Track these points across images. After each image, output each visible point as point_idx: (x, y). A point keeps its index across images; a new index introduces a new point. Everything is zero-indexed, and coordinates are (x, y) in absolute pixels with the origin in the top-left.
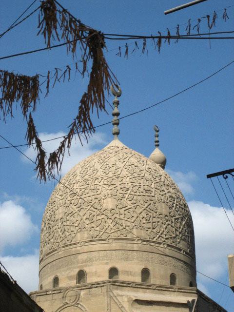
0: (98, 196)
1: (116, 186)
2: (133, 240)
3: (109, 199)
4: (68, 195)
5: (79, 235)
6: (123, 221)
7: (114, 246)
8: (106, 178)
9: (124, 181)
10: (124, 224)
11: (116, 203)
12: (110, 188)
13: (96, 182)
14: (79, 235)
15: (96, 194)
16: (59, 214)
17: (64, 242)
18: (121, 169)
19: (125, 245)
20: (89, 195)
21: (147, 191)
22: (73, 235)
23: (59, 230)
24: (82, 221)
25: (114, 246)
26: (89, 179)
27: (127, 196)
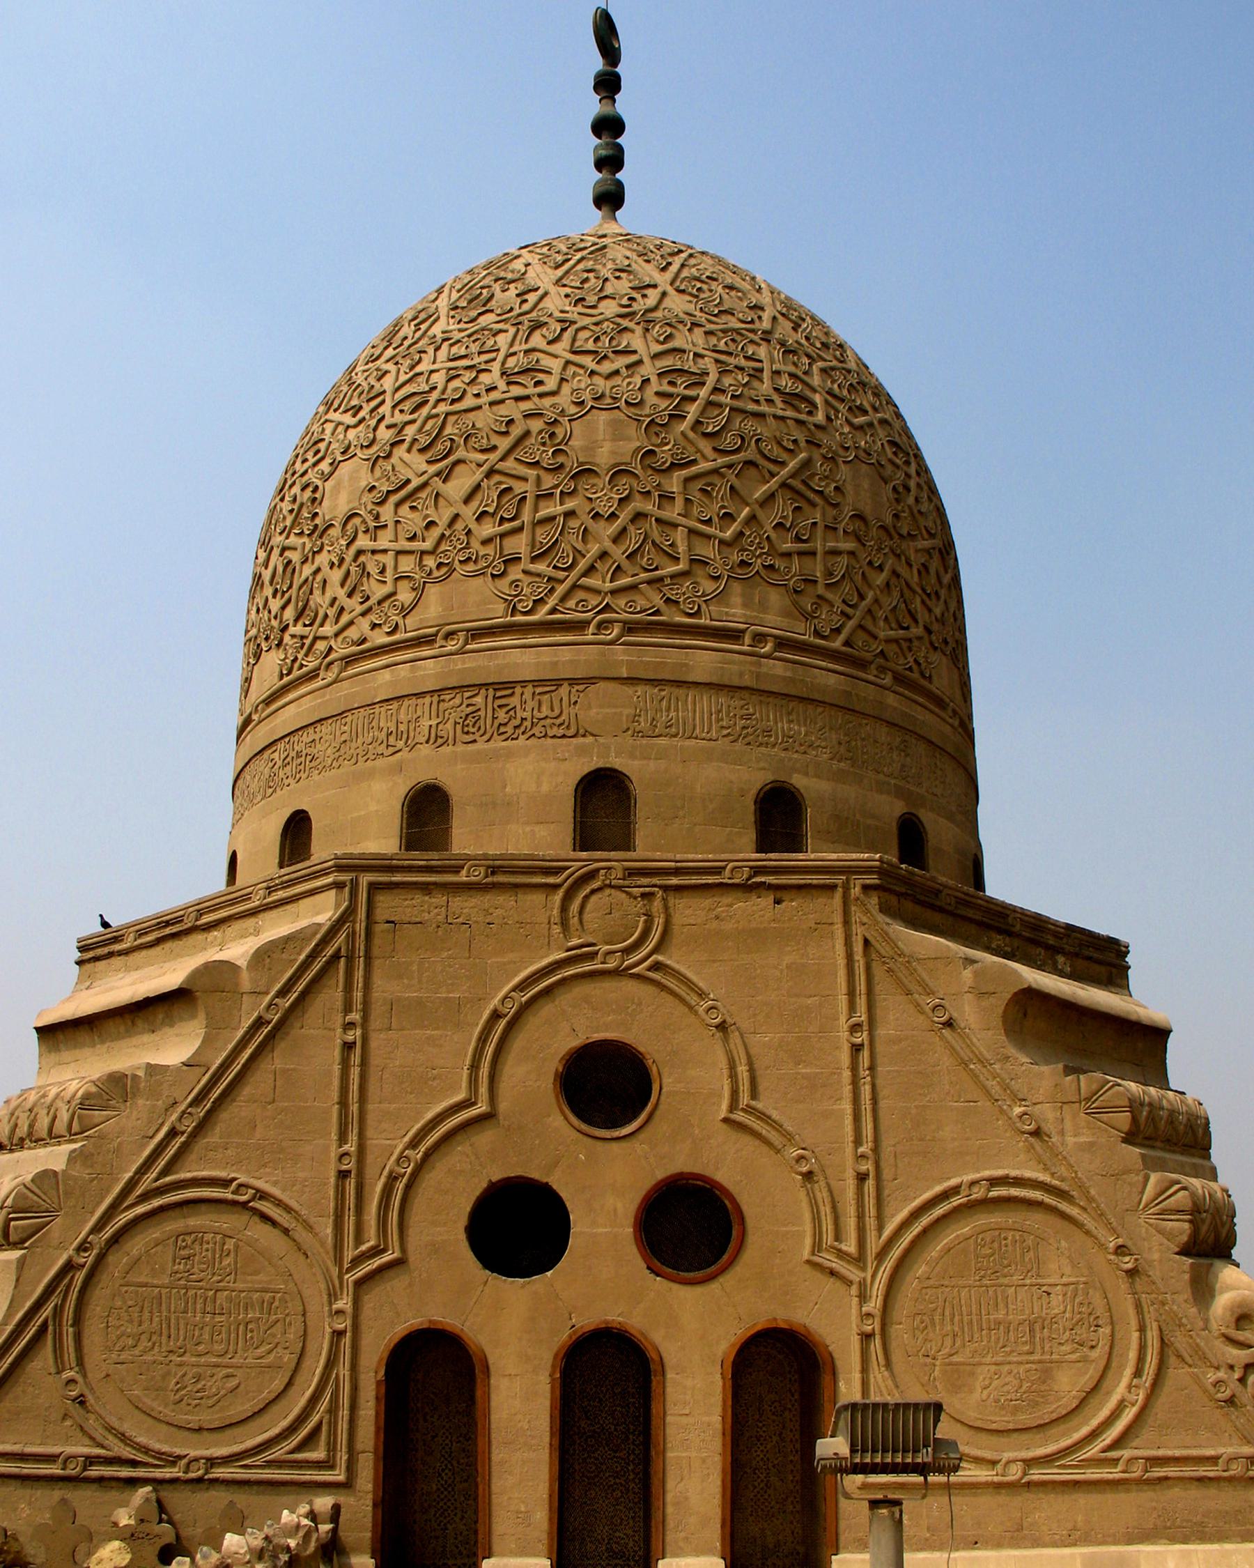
0: (547, 402)
1: (633, 358)
4: (389, 404)
6: (680, 536)
7: (623, 658)
8: (587, 321)
9: (676, 343)
10: (682, 548)
11: (635, 440)
12: (607, 367)
13: (537, 340)
15: (531, 390)
17: (353, 633)
18: (660, 290)
20: (495, 395)
21: (792, 399)
22: (405, 596)
24: (459, 526)
25: (623, 658)
27: (693, 410)
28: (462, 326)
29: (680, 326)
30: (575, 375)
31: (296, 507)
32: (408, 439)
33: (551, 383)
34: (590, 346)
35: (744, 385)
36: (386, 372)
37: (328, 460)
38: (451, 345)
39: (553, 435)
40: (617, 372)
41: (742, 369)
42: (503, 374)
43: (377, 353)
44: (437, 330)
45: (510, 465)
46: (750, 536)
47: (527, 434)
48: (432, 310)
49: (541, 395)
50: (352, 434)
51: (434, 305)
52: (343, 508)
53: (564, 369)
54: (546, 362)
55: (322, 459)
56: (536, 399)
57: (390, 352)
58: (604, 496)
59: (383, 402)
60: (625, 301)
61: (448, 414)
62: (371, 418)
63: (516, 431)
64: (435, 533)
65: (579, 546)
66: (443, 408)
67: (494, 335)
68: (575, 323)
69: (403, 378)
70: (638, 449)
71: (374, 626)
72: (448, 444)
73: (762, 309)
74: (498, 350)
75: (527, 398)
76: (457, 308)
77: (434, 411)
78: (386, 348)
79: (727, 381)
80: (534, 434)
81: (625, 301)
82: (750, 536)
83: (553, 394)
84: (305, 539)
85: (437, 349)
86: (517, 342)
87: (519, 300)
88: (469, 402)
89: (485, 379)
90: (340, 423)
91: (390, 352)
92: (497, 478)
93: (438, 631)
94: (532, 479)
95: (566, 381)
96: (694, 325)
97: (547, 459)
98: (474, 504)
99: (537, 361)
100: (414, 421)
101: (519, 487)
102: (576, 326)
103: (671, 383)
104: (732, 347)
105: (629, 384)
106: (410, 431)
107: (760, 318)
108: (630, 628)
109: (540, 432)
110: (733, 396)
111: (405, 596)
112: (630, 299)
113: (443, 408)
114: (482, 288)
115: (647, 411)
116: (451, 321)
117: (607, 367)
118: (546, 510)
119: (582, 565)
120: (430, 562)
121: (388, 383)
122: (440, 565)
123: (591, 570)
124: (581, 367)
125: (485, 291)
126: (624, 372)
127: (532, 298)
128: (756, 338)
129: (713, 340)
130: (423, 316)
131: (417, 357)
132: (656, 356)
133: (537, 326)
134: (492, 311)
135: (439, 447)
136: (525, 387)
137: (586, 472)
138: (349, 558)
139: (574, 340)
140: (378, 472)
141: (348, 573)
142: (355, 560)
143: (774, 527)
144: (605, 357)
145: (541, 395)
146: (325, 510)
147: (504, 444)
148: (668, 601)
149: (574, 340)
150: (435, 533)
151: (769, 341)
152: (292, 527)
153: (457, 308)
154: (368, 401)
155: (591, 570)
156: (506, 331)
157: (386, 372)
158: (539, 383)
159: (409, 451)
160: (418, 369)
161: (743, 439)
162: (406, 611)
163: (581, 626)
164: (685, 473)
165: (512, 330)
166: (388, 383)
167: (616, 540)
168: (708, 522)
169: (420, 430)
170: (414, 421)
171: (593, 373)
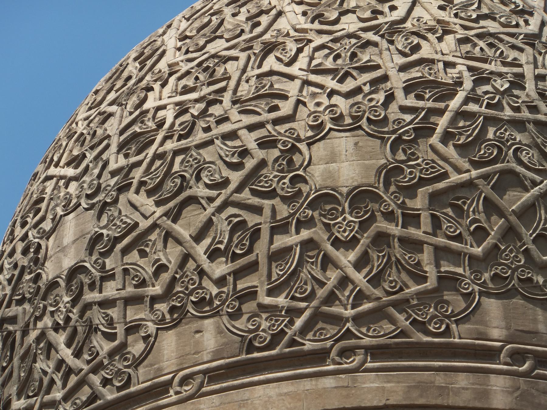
0: (282, 128)
2: (491, 354)
3: (343, 142)
4: (114, 148)
5: (169, 344)
6: (426, 257)
8: (326, 38)
10: (430, 269)
12: (349, 85)
13: (271, 63)
14: (169, 344)
15: (266, 116)
16: (63, 250)
19: (440, 379)
20: (226, 128)
22: (137, 348)
23: (60, 339)
24: (191, 265)
26: (233, 53)
27: (443, 122)
28: (190, 56)
29: (429, 35)
30: (314, 95)
31: (16, 273)
32: (135, 182)
33: (286, 108)
34: (329, 64)
35: (503, 93)
36: (111, 115)
37: (50, 216)
38: (180, 79)
39: (290, 162)
40: (358, 90)
41: (500, 75)
42: (234, 103)
43: (99, 99)
44: (163, 65)
45: (246, 196)
46: (505, 250)
47: (263, 164)
48: (159, 43)
49: (276, 122)
50: (73, 187)
51: (160, 40)
52: (68, 262)
53: (301, 90)
54: (280, 85)
55: (43, 219)
56: (269, 127)
57: (112, 96)
58: (347, 221)
59: (108, 146)
60: (367, 14)
61: (176, 153)
62: (96, 167)
63: (250, 164)
64: (165, 277)
65: (320, 277)
66: (170, 145)
67: (225, 63)
68: (310, 41)
69: (125, 122)
70: (384, 166)
71: (106, 382)
72: (178, 181)
73: (531, 14)
74: (229, 78)
75: (260, 125)
76: (186, 37)
77: (161, 150)
78: (108, 92)
79: (481, 89)
80: (270, 163)
81: (367, 14)
82: (505, 250)
83: (290, 118)
84: (27, 306)
85: (163, 86)
86: (249, 69)
87: (250, 23)
88: (199, 136)
89: (216, 110)
90: (61, 178)
91: (112, 96)
92: (231, 210)
93: (173, 378)
94: (267, 212)
95: (305, 90)
96: (446, 32)
97: (284, 186)
98: (207, 242)
99: (272, 86)
100: (138, 164)
101: (252, 220)
102: (313, 45)
103: (419, 97)
104: (490, 52)
105: (371, 100)
106: (137, 174)
107: (527, 22)
108: (375, 352)
109: (276, 160)
110: (489, 106)
111: (137, 348)
112: (373, 12)
113: (170, 145)
114: (212, 15)
115: (390, 127)
116: (178, 53)
117: (349, 85)
118: (282, 241)
119: (321, 293)
120: (163, 307)
121: (113, 127)
122: (172, 310)
123: (331, 299)
124: (321, 87)
125: (214, 18)
126: (367, 89)
127: (264, 20)
128: (518, 42)
129: (467, 47)
130: (147, 51)
131: (142, 95)
132: (403, 68)
133: (269, 49)
134: (221, 37)
135: (169, 185)
136: (259, 114)
137: (325, 199)
138: (74, 316)
139: (312, 58)
140: (104, 220)
141: (75, 331)
142: (81, 316)
143: (534, 241)
144: (347, 74)
145: (276, 122)
146: (49, 271)
147: (236, 177)
148: (414, 322)
149: (312, 58)
150: (165, 277)
151: (533, 46)
152: (12, 295)
153: (186, 37)
154: (92, 148)
155: (331, 299)
156: (236, 59)
157: (111, 115)
158: (275, 108)
159: (137, 192)
160: (146, 106)
161: (500, 150)
162: (137, 363)
163: (320, 356)
164: (430, 189)
165: (243, 56)
166: (113, 127)
167: (358, 265)
168: (459, 238)
169: (147, 171)
170: (138, 164)
171: (332, 93)
